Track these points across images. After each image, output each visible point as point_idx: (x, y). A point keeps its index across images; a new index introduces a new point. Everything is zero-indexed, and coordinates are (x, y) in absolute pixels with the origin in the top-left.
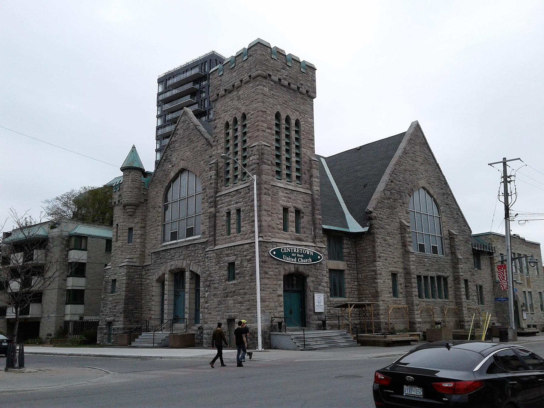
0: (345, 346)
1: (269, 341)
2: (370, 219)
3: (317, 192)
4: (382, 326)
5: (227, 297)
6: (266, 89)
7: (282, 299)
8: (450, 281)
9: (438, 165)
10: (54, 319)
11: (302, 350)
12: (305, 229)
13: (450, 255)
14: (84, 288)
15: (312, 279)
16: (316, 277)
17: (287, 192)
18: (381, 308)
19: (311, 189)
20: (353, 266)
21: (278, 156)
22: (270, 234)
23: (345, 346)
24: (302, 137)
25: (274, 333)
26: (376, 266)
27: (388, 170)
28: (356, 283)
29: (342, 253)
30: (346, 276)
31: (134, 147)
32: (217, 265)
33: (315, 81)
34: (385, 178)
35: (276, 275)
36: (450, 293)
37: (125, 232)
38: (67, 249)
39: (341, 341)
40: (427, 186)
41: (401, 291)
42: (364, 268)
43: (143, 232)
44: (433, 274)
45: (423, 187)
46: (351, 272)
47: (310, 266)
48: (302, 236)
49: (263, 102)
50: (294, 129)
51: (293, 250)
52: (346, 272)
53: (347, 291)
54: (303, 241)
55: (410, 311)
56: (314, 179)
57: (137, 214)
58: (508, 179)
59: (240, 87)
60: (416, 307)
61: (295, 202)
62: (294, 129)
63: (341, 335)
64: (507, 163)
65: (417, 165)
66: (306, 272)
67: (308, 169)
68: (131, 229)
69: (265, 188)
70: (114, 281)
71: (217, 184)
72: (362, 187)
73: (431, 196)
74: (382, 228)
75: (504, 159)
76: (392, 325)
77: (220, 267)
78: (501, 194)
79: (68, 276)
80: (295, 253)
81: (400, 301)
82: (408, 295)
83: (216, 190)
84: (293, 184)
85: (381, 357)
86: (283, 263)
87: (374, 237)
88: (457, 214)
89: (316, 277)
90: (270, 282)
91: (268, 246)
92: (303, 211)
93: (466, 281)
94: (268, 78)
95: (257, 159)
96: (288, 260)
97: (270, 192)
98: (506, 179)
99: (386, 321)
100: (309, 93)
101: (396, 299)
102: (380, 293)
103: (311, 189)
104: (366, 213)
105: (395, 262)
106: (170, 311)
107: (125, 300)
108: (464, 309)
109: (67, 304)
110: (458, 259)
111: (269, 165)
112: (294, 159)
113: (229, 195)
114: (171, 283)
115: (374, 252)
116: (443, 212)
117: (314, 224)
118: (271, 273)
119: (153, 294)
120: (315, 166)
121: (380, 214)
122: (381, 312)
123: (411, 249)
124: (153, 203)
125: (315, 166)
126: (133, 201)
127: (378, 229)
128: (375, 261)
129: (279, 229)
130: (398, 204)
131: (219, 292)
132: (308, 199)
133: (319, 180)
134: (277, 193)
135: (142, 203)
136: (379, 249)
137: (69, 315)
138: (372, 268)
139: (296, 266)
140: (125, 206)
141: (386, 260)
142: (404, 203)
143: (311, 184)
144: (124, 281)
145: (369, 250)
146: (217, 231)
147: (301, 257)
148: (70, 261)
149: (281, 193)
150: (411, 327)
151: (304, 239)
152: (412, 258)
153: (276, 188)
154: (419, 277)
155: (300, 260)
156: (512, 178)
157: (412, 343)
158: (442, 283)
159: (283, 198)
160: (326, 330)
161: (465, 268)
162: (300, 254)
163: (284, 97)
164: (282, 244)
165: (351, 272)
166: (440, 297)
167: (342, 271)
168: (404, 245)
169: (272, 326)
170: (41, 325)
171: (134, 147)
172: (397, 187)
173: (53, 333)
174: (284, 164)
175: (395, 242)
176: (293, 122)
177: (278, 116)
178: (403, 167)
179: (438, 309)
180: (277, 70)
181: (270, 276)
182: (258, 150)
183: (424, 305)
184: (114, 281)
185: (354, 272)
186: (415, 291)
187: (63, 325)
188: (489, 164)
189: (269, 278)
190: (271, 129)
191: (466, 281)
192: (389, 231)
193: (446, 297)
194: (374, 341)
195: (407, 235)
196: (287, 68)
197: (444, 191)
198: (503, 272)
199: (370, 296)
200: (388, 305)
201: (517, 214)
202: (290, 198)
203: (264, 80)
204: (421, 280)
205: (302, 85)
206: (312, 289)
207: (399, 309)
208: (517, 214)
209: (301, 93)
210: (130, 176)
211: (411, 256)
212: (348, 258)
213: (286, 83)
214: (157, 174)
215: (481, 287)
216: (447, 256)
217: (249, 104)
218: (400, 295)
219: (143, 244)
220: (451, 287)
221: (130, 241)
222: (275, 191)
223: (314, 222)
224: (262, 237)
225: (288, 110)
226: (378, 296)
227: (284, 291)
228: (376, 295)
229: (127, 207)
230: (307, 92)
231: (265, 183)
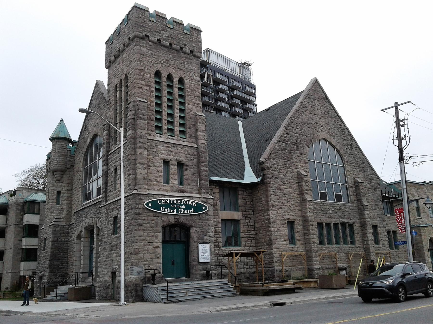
0: (219, 297)
1: (141, 293)
2: (263, 169)
3: (203, 145)
4: (276, 274)
5: (112, 250)
6: (144, 49)
7: (160, 251)
8: (356, 227)
9: (340, 118)
10: (10, 274)
11: (165, 303)
12: (189, 181)
13: (356, 202)
14: (37, 247)
15: (195, 229)
16: (201, 227)
17: (168, 145)
18: (275, 255)
19: (196, 143)
20: (249, 216)
21: (159, 112)
22: (146, 187)
23: (219, 297)
24: (187, 93)
25: (146, 285)
26: (269, 215)
27: (284, 124)
28: (253, 232)
29: (238, 203)
30: (241, 226)
31: (62, 120)
32: (106, 220)
33: (200, 42)
34: (281, 130)
35: (153, 227)
36: (356, 239)
37: (54, 195)
38: (22, 213)
39: (218, 291)
40: (329, 138)
41: (299, 238)
42: (260, 218)
43: (69, 195)
44: (337, 221)
45: (324, 139)
46: (247, 221)
47: (193, 217)
48: (186, 187)
49: (140, 61)
50: (177, 86)
51: (173, 201)
52: (242, 222)
53: (243, 240)
54: (186, 192)
55: (309, 259)
56: (199, 133)
57: (63, 178)
58: (401, 123)
59: (124, 50)
60: (314, 254)
61: (176, 155)
62: (177, 86)
63: (220, 285)
64: (399, 107)
65: (317, 118)
66: (189, 222)
67: (194, 123)
68: (59, 193)
69: (140, 142)
70: (45, 239)
71: (109, 143)
72: (264, 141)
73: (334, 147)
74: (276, 178)
75: (396, 103)
76: (287, 273)
77: (108, 222)
78: (395, 138)
79: (23, 237)
80: (175, 204)
81: (297, 248)
82: (307, 242)
83: (108, 149)
84: (176, 138)
85: (227, 310)
86: (160, 215)
87: (267, 187)
88: (363, 163)
89: (201, 227)
90: (146, 234)
91: (142, 198)
92: (187, 163)
93: (375, 227)
94: (147, 39)
95: (133, 115)
96: (167, 211)
97: (146, 146)
98: (399, 123)
99: (280, 268)
100: (194, 53)
101: (293, 246)
102: (273, 241)
103: (196, 143)
104: (259, 164)
105: (291, 210)
106: (85, 266)
107: (51, 256)
108: (372, 254)
109: (21, 261)
110: (364, 205)
111: (145, 120)
112: (177, 114)
113: (116, 153)
114: (86, 240)
115: (267, 201)
116: (347, 162)
117: (200, 176)
118: (146, 225)
119: (75, 250)
120: (200, 121)
121: (274, 164)
122: (275, 260)
123: (308, 197)
124: (77, 168)
125: (200, 121)
126: (58, 167)
127: (271, 178)
128: (268, 210)
129: (158, 182)
130: (295, 155)
131: (107, 246)
132: (194, 152)
133: (205, 134)
134: (156, 146)
135: (68, 168)
136: (272, 198)
137: (23, 271)
138: (266, 217)
139: (176, 217)
140: (53, 172)
141: (281, 208)
142: (301, 154)
143: (196, 138)
144: (50, 239)
145: (263, 199)
146: (108, 188)
147: (182, 208)
148: (24, 224)
149: (160, 147)
150: (310, 272)
151: (189, 191)
152: (310, 206)
153: (155, 142)
154: (320, 225)
155: (181, 211)
156: (406, 122)
157: (296, 291)
158: (348, 228)
159: (163, 152)
160: (211, 279)
161: (373, 215)
162: (181, 205)
163: (165, 57)
164: (160, 196)
165: (247, 221)
166: (345, 243)
167: (238, 221)
168: (302, 193)
169: (145, 278)
170: (2, 280)
171: (62, 120)
172: (294, 139)
173: (9, 287)
174: (165, 120)
175: (291, 191)
176: (176, 80)
177: (158, 74)
178: (300, 120)
179: (343, 255)
180: (156, 32)
181: (145, 228)
182: (134, 106)
183: (327, 251)
184: (45, 239)
185: (251, 221)
186: (315, 238)
187: (18, 280)
188: (381, 110)
189: (143, 230)
190: (149, 86)
191: (375, 227)
192: (285, 180)
193: (352, 243)
194: (254, 290)
195: (304, 184)
196: (168, 30)
197: (348, 142)
198: (401, 215)
199: (265, 244)
200: (282, 251)
201: (412, 157)
202: (172, 152)
203: (142, 41)
204: (323, 227)
205: (185, 45)
206: (196, 239)
207: (296, 256)
208: (412, 157)
209: (185, 53)
210: (57, 145)
211: (308, 204)
212: (243, 209)
213: (167, 43)
214: (80, 141)
215: (395, 232)
216: (353, 203)
217: (130, 64)
218: (298, 242)
219: (70, 206)
220: (358, 233)
221: (58, 203)
222: (154, 144)
223: (199, 174)
224: (137, 189)
225: (169, 68)
226: (271, 244)
227: (163, 242)
228: (270, 243)
229: (55, 173)
230: (192, 52)
231: (141, 137)
